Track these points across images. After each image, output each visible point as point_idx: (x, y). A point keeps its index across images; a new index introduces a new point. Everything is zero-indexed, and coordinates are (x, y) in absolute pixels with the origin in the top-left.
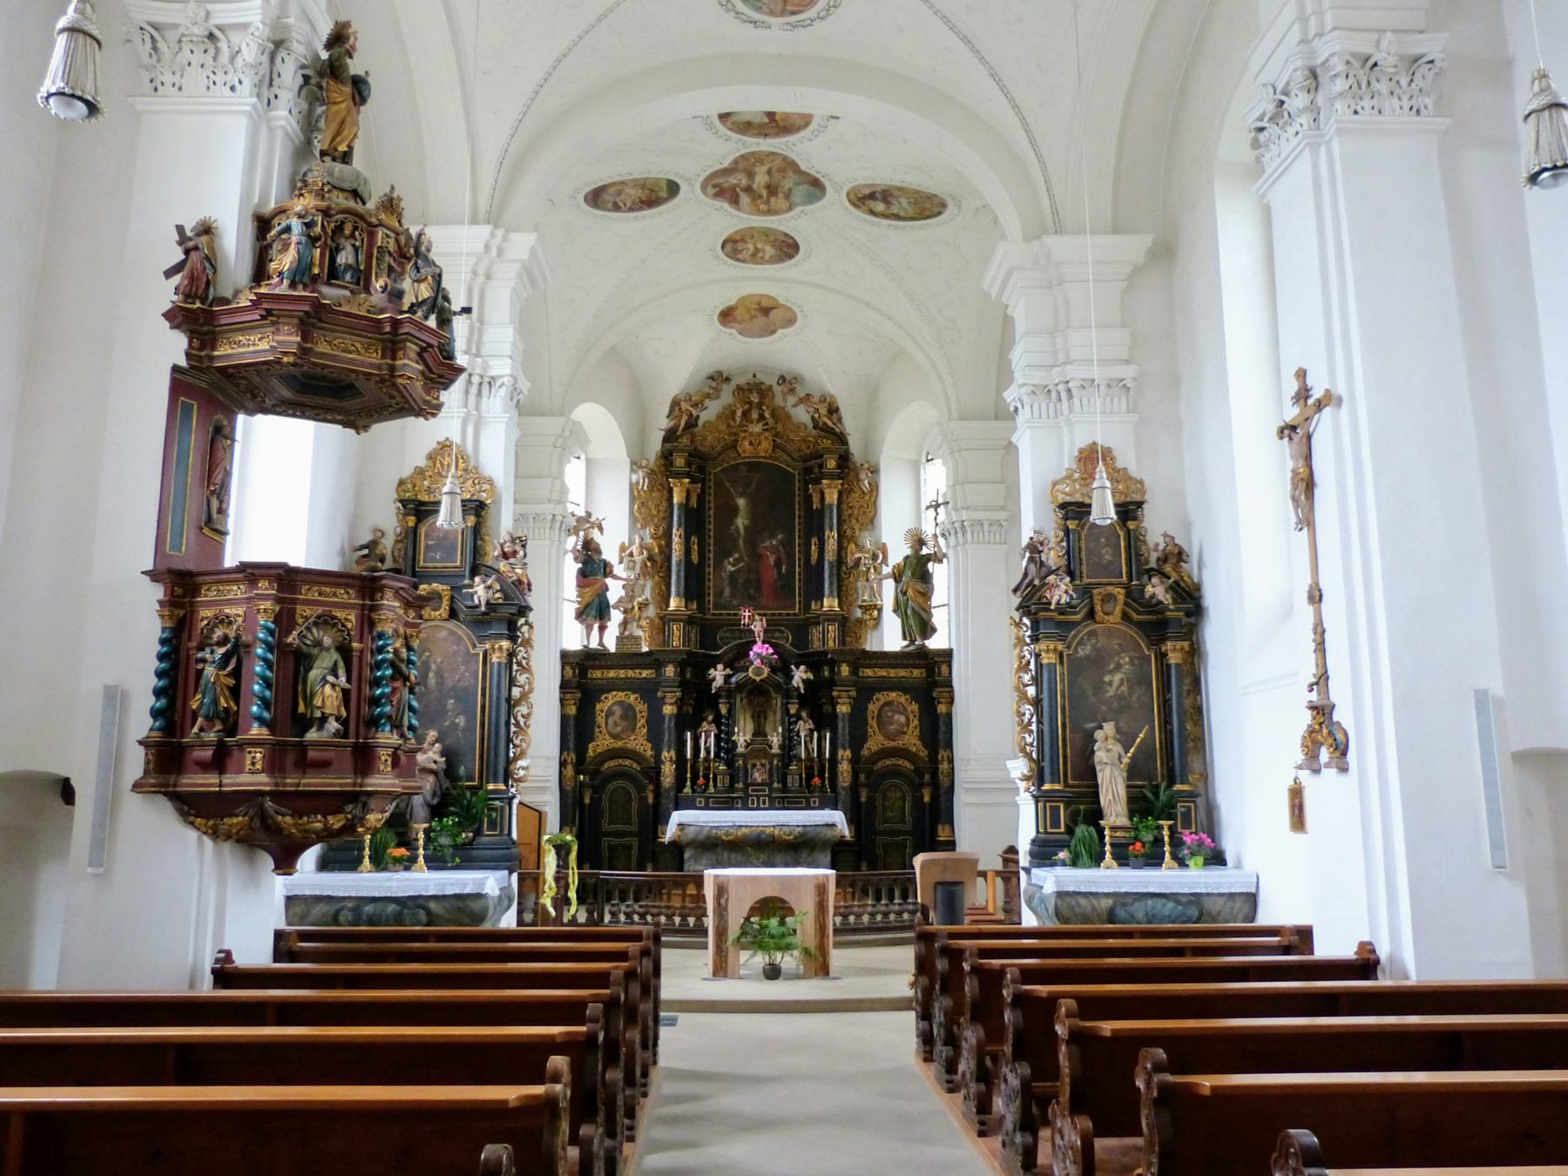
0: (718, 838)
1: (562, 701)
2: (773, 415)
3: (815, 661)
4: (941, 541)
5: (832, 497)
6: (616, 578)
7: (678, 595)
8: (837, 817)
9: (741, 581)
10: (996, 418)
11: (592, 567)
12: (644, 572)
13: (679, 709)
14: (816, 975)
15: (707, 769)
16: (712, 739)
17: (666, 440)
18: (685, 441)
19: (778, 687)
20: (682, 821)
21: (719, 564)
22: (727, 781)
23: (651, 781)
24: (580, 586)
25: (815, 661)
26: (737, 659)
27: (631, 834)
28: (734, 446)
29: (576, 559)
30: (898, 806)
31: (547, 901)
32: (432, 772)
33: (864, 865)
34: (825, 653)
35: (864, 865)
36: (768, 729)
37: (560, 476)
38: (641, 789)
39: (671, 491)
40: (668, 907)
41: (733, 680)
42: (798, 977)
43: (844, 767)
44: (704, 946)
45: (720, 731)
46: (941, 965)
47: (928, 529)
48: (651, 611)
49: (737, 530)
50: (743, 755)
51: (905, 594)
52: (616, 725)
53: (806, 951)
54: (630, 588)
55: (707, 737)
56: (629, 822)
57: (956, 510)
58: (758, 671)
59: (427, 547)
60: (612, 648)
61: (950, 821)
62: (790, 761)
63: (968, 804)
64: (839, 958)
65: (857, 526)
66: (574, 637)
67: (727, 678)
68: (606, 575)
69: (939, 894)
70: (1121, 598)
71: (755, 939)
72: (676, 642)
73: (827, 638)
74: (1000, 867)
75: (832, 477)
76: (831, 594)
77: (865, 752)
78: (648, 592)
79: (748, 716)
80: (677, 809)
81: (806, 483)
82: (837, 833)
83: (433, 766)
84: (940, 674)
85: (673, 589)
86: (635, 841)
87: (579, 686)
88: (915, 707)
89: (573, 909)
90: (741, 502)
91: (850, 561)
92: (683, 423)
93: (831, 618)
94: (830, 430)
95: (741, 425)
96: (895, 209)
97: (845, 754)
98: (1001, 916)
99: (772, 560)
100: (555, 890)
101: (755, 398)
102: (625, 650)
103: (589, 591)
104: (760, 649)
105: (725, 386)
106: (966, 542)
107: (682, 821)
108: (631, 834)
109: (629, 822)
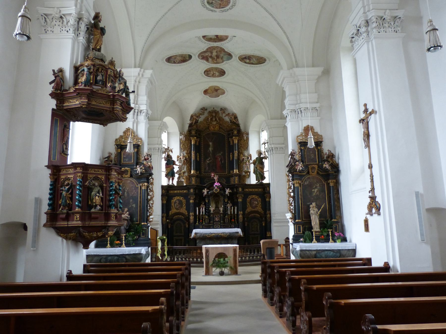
1: (162, 199)
2: (219, 119)
3: (232, 187)
4: (266, 153)
5: (236, 141)
6: (176, 165)
7: (194, 169)
10: (281, 119)
11: (170, 162)
12: (184, 163)
13: (195, 201)
15: (203, 218)
17: (189, 127)
18: (195, 127)
19: (222, 195)
21: (205, 161)
23: (187, 221)
25: (232, 187)
28: (208, 128)
29: (165, 160)
32: (126, 220)
33: (247, 243)
34: (235, 185)
35: (247, 243)
36: (219, 206)
37: (160, 137)
43: (241, 216)
44: (203, 267)
45: (206, 207)
46: (269, 271)
48: (186, 174)
49: (210, 151)
50: (212, 213)
51: (256, 168)
52: (177, 206)
53: (231, 268)
54: (180, 168)
55: (203, 209)
57: (270, 144)
58: (216, 190)
59: (124, 158)
60: (175, 184)
66: (165, 182)
67: (208, 192)
69: (268, 251)
70: (317, 168)
71: (217, 264)
75: (236, 136)
76: (236, 169)
77: (246, 212)
81: (229, 138)
83: (127, 218)
87: (167, 195)
88: (260, 199)
89: (166, 257)
90: (211, 143)
93: (236, 175)
96: (252, 62)
101: (214, 115)
104: (217, 184)
105: (205, 111)
106: (273, 153)
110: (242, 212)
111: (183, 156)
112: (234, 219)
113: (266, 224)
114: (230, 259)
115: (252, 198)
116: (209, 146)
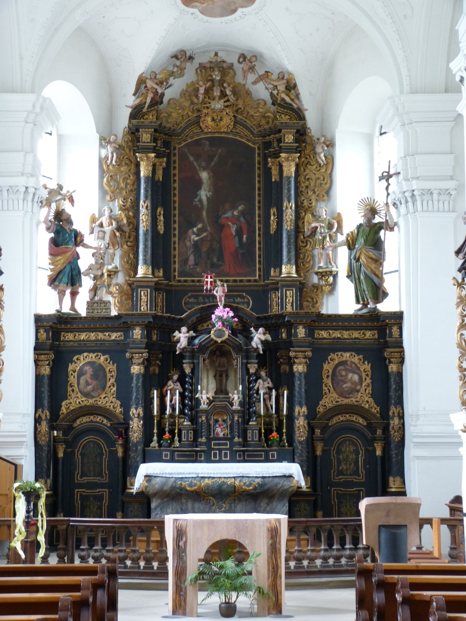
0: (182, 489)
1: (36, 362)
2: (234, 92)
3: (273, 324)
4: (392, 209)
5: (290, 169)
7: (145, 263)
8: (294, 469)
9: (204, 249)
10: (446, 91)
11: (63, 236)
12: (113, 242)
13: (146, 368)
14: (269, 614)
15: (173, 424)
16: (177, 397)
17: (133, 116)
18: (151, 117)
19: (238, 349)
20: (150, 473)
21: (183, 234)
22: (191, 435)
23: (120, 435)
25: (273, 324)
27: (102, 486)
28: (197, 122)
29: (48, 229)
30: (351, 458)
31: (17, 544)
33: (320, 513)
34: (282, 316)
35: (320, 513)
36: (230, 387)
37: (32, 150)
39: (138, 165)
40: (134, 551)
41: (197, 341)
42: (251, 615)
43: (301, 423)
44: (165, 588)
45: (184, 389)
46: (379, 598)
47: (380, 200)
48: (120, 279)
49: (201, 201)
50: (205, 411)
51: (358, 260)
52: (87, 384)
53: (260, 590)
54: (100, 257)
55: (172, 395)
56: (100, 474)
57: (407, 180)
58: (220, 333)
60: (83, 312)
62: (250, 417)
63: (418, 458)
64: (289, 598)
65: (313, 197)
66: (49, 302)
67: (191, 340)
68: (77, 244)
69: (383, 536)
71: (210, 580)
72: (144, 307)
73: (286, 303)
74: (446, 514)
75: (289, 150)
76: (289, 262)
77: (320, 409)
78: (117, 261)
79: (211, 375)
80: (144, 462)
81: (265, 157)
84: (391, 335)
85: (141, 257)
86: (106, 492)
87: (52, 348)
88: (367, 367)
89: (42, 552)
90: (204, 175)
91: (307, 230)
92: (149, 100)
93: (289, 283)
95: (204, 102)
97: (301, 411)
98: (445, 563)
99: (233, 229)
100: (24, 534)
101: (217, 76)
102: (96, 314)
103: (61, 260)
104: (222, 312)
105: (188, 64)
106: (415, 211)
107: (150, 473)
108: (102, 486)
109: (100, 474)
110: (304, 409)
113: (386, 449)
114: (258, 563)
115: (341, 363)
116: (198, 184)
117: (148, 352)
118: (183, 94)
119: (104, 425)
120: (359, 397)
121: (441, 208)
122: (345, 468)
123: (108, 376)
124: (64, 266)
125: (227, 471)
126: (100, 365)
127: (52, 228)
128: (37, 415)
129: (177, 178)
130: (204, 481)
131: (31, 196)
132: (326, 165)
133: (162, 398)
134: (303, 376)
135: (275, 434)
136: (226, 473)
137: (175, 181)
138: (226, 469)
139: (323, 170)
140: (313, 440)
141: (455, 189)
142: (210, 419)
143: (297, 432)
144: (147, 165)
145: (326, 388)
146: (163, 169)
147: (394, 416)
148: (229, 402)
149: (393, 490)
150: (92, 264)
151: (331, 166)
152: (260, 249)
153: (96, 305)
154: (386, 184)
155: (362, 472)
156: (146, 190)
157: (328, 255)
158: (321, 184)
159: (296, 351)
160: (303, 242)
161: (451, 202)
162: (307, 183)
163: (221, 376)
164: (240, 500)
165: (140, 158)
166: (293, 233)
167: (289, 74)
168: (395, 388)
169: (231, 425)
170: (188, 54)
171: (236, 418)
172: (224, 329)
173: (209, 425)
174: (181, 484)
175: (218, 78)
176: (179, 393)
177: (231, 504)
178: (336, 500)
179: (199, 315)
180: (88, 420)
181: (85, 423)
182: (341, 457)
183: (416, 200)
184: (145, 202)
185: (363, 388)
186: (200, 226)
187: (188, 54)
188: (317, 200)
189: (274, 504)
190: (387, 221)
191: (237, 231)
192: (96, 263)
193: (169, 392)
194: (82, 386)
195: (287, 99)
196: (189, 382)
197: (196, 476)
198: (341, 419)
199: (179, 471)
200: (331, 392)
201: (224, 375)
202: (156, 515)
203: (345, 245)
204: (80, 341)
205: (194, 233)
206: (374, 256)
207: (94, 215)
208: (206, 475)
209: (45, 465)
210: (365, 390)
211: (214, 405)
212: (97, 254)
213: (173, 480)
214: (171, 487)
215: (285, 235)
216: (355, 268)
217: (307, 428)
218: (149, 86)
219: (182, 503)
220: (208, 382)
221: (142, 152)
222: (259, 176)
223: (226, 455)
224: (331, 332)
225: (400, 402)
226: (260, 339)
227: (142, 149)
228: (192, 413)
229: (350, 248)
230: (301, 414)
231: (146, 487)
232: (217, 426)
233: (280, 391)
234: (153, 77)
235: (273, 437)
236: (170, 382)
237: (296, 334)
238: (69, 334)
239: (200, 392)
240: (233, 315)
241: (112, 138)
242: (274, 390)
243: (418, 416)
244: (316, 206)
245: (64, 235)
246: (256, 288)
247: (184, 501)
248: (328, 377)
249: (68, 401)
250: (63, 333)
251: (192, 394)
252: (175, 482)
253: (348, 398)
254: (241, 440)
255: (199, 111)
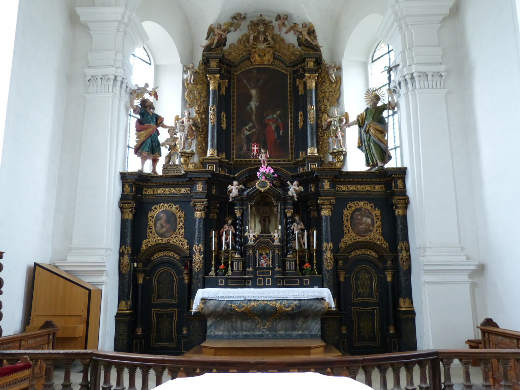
0: (232, 310)
2: (273, 39)
5: (312, 84)
6: (164, 127)
7: (212, 147)
8: (326, 293)
13: (207, 214)
15: (227, 258)
16: (230, 237)
19: (278, 197)
21: (239, 130)
22: (241, 266)
23: (186, 267)
24: (138, 130)
25: (305, 180)
26: (252, 176)
27: (173, 306)
36: (271, 229)
38: (180, 273)
41: (245, 193)
43: (328, 255)
49: (251, 108)
50: (252, 246)
51: (367, 132)
52: (162, 227)
56: (171, 297)
58: (263, 184)
60: (160, 171)
61: (409, 295)
63: (428, 283)
65: (328, 104)
66: (135, 164)
67: (241, 191)
75: (311, 71)
76: (312, 145)
77: (342, 245)
82: (325, 305)
84: (396, 186)
85: (209, 143)
87: (134, 198)
88: (377, 212)
90: (253, 92)
91: (324, 124)
92: (216, 41)
94: (309, 45)
97: (328, 246)
99: (273, 127)
105: (243, 23)
106: (414, 88)
108: (173, 306)
109: (171, 297)
110: (330, 245)
111: (189, 118)
112: (311, 262)
113: (396, 276)
115: (357, 210)
116: (250, 97)
117: (207, 201)
118: (239, 41)
119: (175, 258)
120: (372, 236)
121: (434, 86)
122: (362, 291)
123: (178, 220)
124: (146, 138)
125: (270, 295)
126: (172, 212)
127: (137, 111)
128: (121, 250)
129: (235, 94)
130: (250, 303)
131: (119, 83)
132: (336, 82)
133: (219, 237)
134: (329, 218)
135: (307, 264)
136: (269, 297)
137: (234, 96)
138: (274, 293)
139: (334, 86)
140: (337, 269)
141: (445, 71)
142: (256, 253)
143: (325, 263)
144: (214, 83)
145: (346, 229)
146: (226, 88)
147: (402, 250)
148: (271, 239)
149: (403, 309)
150: (168, 139)
151: (339, 83)
152: (291, 139)
153: (169, 167)
154: (388, 75)
155: (376, 295)
156: (213, 99)
157: (339, 141)
158: (333, 95)
159: (323, 200)
160: (321, 133)
161: (442, 82)
162: (323, 95)
163: (264, 220)
164: (280, 319)
165: (210, 78)
166: (315, 126)
167: (310, 23)
168: (402, 228)
169: (272, 257)
170: (242, 17)
171: (277, 252)
172: (267, 181)
173: (255, 258)
174: (231, 306)
175: (262, 30)
176: (232, 233)
177: (273, 323)
178: (356, 317)
179: (247, 175)
180: (163, 255)
181: (160, 257)
182: (359, 282)
183: (415, 81)
184: (212, 107)
185: (375, 228)
186: (250, 125)
187: (242, 17)
188: (330, 106)
189: (309, 322)
190: (389, 102)
191: (275, 128)
192: (171, 137)
193: (224, 232)
194: (158, 229)
195: (309, 39)
196: (239, 224)
197: (244, 299)
198: (358, 253)
199: (230, 295)
200: (350, 231)
201: (267, 220)
202: (211, 331)
203: (356, 124)
204: (157, 194)
205: (247, 130)
206: (380, 129)
207: (178, 116)
208: (252, 299)
209: (126, 290)
210: (377, 230)
211: (259, 241)
212: (171, 130)
213: (224, 302)
214: (223, 308)
215: (309, 128)
216: (365, 138)
217: (333, 260)
218: (216, 33)
219: (232, 322)
220: (255, 225)
221: (211, 74)
222: (290, 92)
223: (269, 281)
224: (349, 186)
225: (406, 238)
226: (295, 189)
227: (211, 72)
228: (241, 248)
229: (360, 127)
230: (328, 249)
231: (202, 309)
232: (262, 258)
233: (310, 232)
234: (219, 27)
235: (306, 267)
236: (226, 226)
237: (323, 186)
238: (149, 190)
239: (248, 231)
240: (273, 172)
241: (191, 66)
242: (306, 231)
243: (425, 248)
244: (329, 110)
245: (148, 116)
246: (289, 166)
247: (234, 320)
248: (347, 220)
249: (147, 240)
250: (145, 189)
251: (241, 233)
252: (226, 304)
253: (364, 236)
254: (280, 269)
255: (249, 51)
